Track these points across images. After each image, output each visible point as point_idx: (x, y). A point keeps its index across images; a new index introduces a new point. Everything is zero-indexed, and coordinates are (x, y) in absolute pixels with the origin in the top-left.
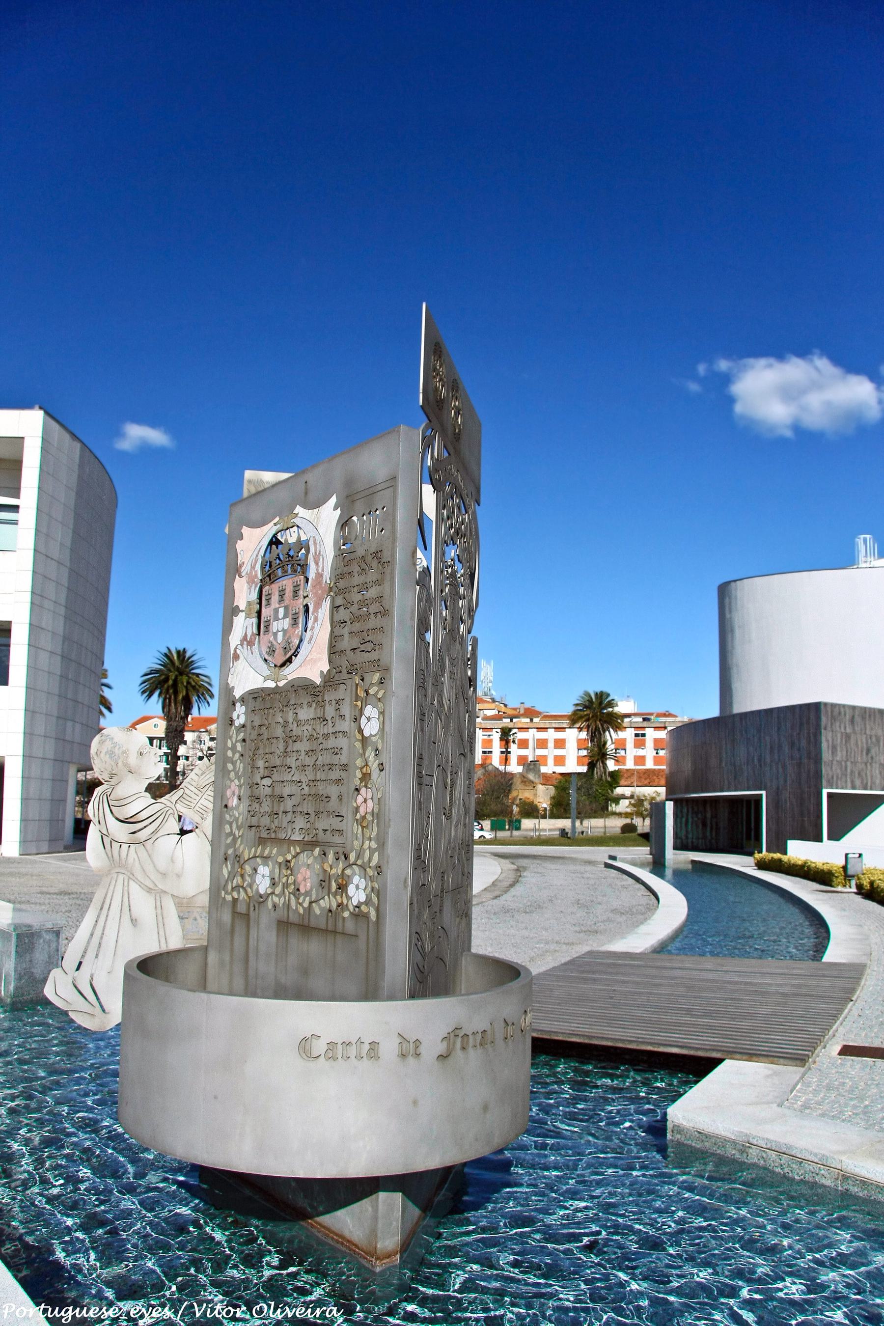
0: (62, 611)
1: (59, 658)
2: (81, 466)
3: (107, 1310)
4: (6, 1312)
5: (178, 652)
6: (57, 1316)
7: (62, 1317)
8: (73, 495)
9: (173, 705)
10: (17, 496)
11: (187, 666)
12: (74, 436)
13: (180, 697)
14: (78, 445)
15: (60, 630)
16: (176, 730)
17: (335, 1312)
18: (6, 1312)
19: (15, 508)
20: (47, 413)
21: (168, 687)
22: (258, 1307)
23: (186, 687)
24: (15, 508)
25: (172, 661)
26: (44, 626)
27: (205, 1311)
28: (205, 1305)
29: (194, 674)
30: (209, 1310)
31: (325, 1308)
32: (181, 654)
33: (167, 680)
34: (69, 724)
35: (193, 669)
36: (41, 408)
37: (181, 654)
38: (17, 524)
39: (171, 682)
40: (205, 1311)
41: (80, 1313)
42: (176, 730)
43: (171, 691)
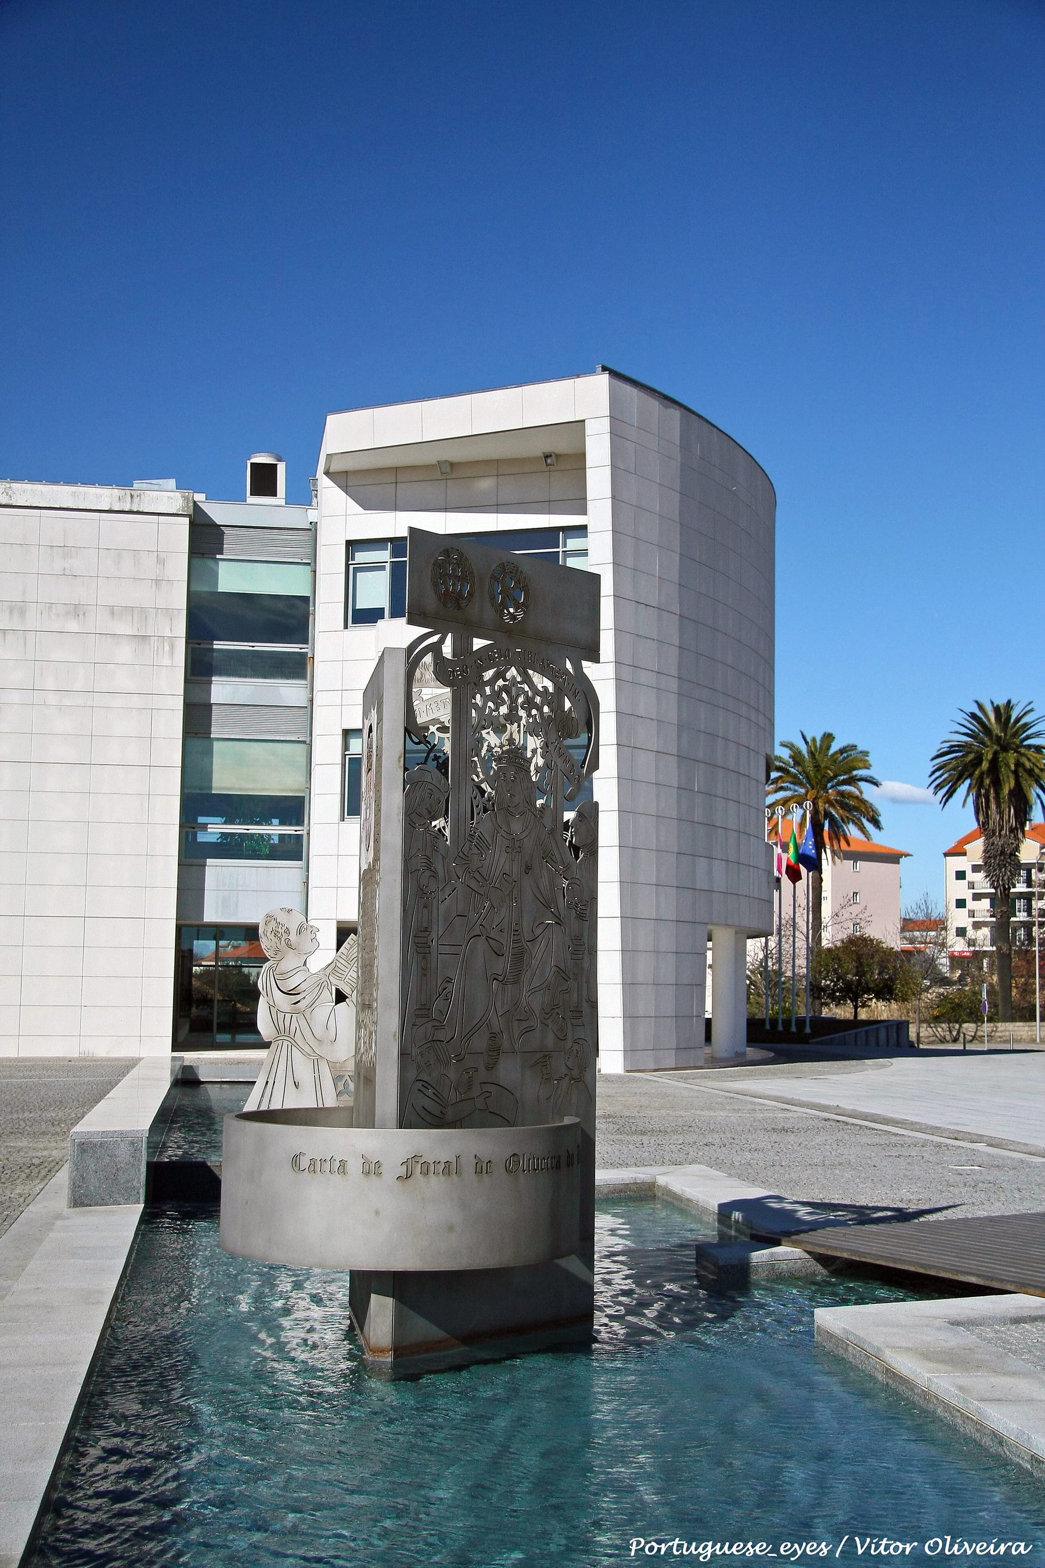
0: (674, 685)
1: (673, 760)
2: (685, 446)
3: (753, 1547)
4: (634, 1548)
5: (997, 710)
6: (694, 1552)
7: (700, 1554)
8: (676, 497)
9: (993, 806)
10: (584, 512)
11: (1015, 734)
12: (668, 400)
13: (1006, 791)
14: (676, 413)
15: (672, 716)
16: (1003, 853)
17: (1022, 1548)
18: (634, 1548)
19: (581, 530)
20: (614, 374)
21: (982, 774)
22: (932, 1542)
23: (1016, 773)
24: (581, 530)
25: (987, 730)
26: (642, 713)
27: (869, 1547)
28: (868, 1540)
29: (1029, 747)
30: (873, 1546)
31: (1010, 1544)
32: (1003, 713)
33: (978, 760)
34: (702, 863)
35: (1028, 738)
36: (604, 369)
37: (1003, 713)
38: (586, 555)
39: (985, 765)
40: (869, 1547)
41: (721, 1549)
42: (1003, 853)
43: (987, 781)
